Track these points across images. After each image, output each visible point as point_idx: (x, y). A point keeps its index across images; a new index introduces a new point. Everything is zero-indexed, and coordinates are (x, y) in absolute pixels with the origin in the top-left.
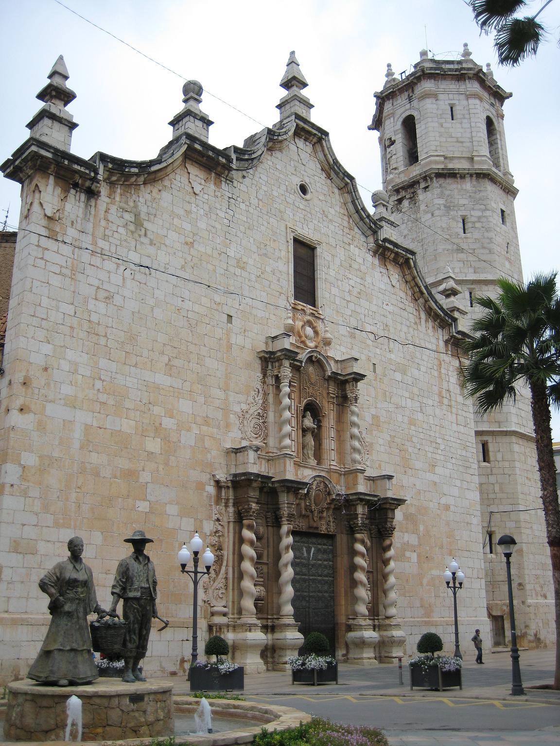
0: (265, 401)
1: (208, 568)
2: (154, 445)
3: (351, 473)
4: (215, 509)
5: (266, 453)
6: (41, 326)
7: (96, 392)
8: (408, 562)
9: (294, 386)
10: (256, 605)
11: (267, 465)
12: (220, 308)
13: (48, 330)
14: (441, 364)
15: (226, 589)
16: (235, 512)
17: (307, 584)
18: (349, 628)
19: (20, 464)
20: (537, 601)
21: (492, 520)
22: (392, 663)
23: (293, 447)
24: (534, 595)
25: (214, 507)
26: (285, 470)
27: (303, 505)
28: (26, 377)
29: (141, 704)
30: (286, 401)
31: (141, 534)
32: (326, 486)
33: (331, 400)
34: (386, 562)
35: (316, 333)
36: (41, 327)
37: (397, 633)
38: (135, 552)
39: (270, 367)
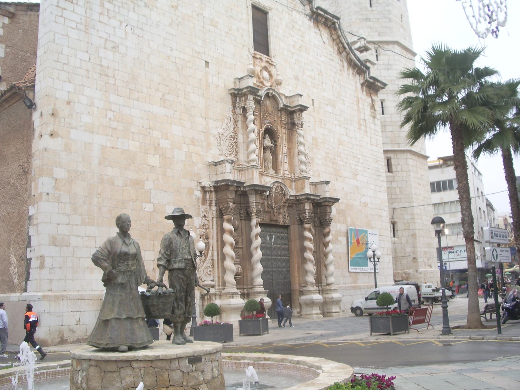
0: (236, 126)
1: (201, 252)
2: (154, 160)
3: (300, 180)
4: (202, 208)
5: (238, 165)
6: (63, 69)
7: (108, 120)
8: (341, 244)
9: (257, 115)
10: (235, 278)
11: (239, 175)
13: (69, 73)
14: (359, 101)
15: (213, 268)
16: (217, 210)
18: (302, 293)
19: (53, 177)
20: (425, 269)
21: (395, 214)
22: (333, 316)
23: (257, 161)
24: (424, 266)
25: (201, 206)
26: (253, 178)
27: (266, 204)
28: (53, 110)
29: (199, 364)
30: (252, 126)
31: (180, 211)
32: (282, 189)
33: (284, 126)
34: (326, 245)
35: (271, 75)
36: (63, 70)
37: (335, 295)
38: (176, 227)
39: (238, 101)
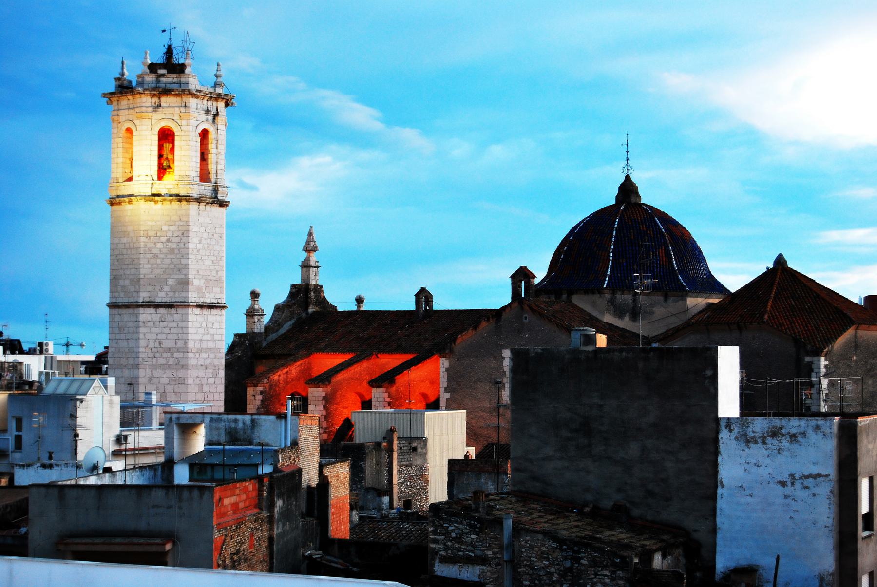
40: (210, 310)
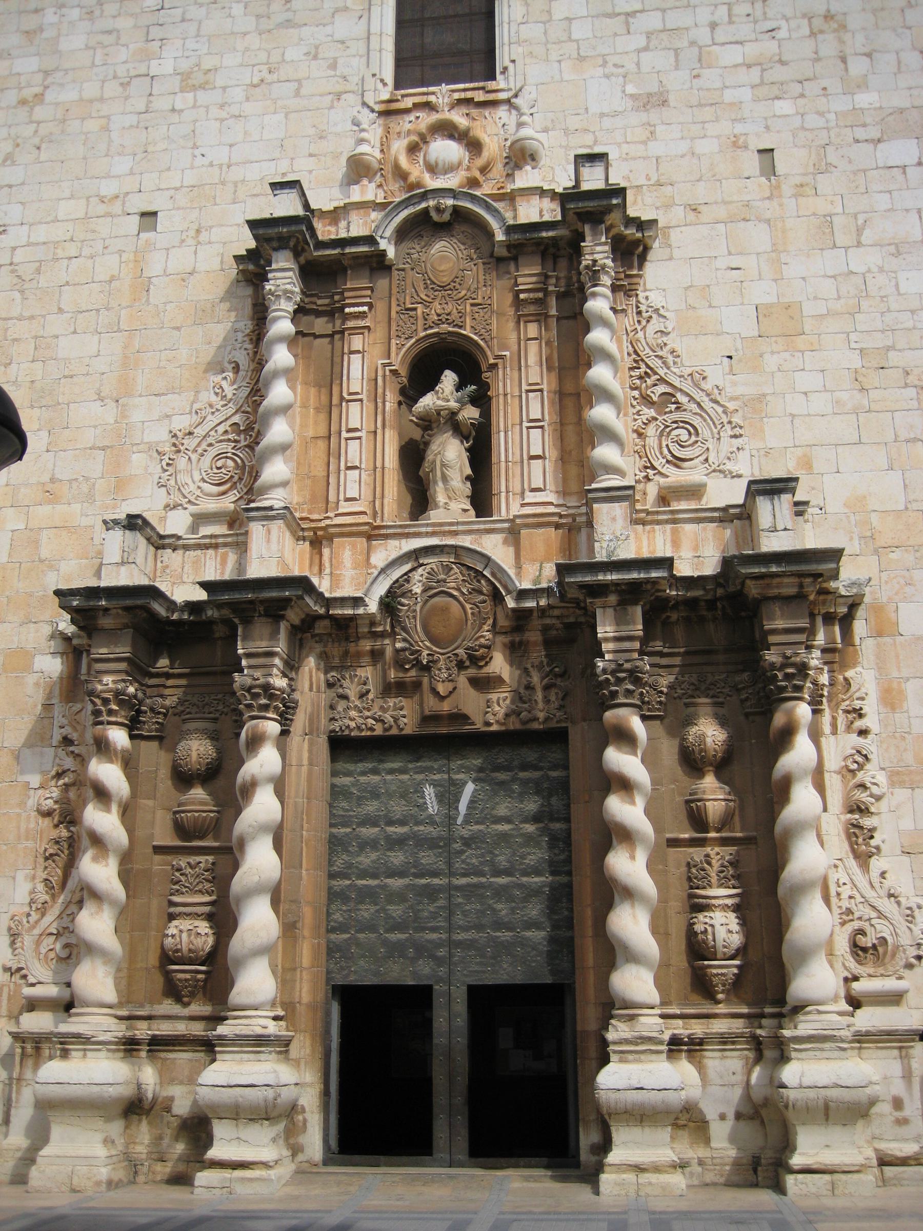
12: (117, 208)
17: (441, 903)
40: (776, 497)
